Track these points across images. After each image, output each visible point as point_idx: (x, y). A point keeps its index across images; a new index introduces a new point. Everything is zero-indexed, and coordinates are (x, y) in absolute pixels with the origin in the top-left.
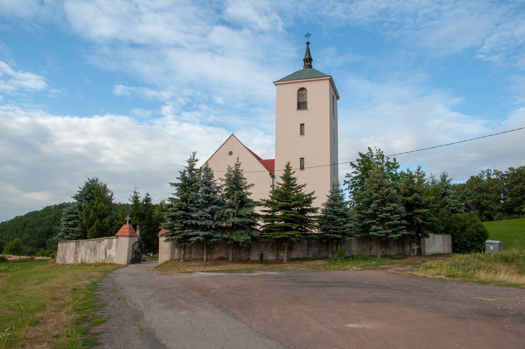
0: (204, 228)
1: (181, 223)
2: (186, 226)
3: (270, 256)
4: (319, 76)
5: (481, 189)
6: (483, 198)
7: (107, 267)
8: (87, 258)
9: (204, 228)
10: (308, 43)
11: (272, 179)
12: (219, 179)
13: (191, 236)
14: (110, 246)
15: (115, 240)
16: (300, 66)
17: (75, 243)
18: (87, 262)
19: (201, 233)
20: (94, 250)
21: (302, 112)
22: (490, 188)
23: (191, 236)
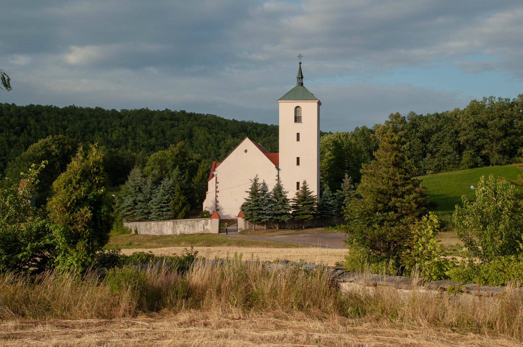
0: (269, 215)
1: (256, 212)
2: (259, 214)
3: (296, 226)
4: (308, 96)
5: (479, 124)
6: (480, 135)
7: (187, 237)
8: (186, 230)
9: (269, 215)
10: (300, 63)
11: (277, 171)
12: (270, 189)
13: (262, 219)
14: (207, 224)
15: (210, 221)
16: (294, 84)
17: (172, 223)
18: (187, 233)
19: (268, 217)
20: (193, 226)
21: (298, 124)
22: (490, 123)
23: (262, 219)
